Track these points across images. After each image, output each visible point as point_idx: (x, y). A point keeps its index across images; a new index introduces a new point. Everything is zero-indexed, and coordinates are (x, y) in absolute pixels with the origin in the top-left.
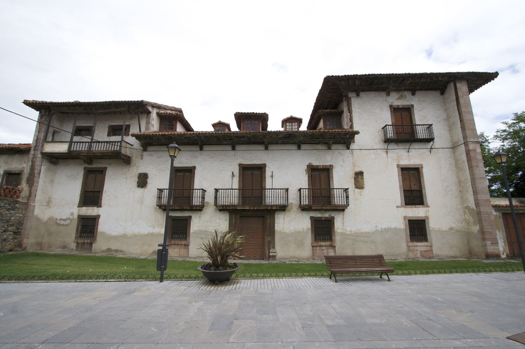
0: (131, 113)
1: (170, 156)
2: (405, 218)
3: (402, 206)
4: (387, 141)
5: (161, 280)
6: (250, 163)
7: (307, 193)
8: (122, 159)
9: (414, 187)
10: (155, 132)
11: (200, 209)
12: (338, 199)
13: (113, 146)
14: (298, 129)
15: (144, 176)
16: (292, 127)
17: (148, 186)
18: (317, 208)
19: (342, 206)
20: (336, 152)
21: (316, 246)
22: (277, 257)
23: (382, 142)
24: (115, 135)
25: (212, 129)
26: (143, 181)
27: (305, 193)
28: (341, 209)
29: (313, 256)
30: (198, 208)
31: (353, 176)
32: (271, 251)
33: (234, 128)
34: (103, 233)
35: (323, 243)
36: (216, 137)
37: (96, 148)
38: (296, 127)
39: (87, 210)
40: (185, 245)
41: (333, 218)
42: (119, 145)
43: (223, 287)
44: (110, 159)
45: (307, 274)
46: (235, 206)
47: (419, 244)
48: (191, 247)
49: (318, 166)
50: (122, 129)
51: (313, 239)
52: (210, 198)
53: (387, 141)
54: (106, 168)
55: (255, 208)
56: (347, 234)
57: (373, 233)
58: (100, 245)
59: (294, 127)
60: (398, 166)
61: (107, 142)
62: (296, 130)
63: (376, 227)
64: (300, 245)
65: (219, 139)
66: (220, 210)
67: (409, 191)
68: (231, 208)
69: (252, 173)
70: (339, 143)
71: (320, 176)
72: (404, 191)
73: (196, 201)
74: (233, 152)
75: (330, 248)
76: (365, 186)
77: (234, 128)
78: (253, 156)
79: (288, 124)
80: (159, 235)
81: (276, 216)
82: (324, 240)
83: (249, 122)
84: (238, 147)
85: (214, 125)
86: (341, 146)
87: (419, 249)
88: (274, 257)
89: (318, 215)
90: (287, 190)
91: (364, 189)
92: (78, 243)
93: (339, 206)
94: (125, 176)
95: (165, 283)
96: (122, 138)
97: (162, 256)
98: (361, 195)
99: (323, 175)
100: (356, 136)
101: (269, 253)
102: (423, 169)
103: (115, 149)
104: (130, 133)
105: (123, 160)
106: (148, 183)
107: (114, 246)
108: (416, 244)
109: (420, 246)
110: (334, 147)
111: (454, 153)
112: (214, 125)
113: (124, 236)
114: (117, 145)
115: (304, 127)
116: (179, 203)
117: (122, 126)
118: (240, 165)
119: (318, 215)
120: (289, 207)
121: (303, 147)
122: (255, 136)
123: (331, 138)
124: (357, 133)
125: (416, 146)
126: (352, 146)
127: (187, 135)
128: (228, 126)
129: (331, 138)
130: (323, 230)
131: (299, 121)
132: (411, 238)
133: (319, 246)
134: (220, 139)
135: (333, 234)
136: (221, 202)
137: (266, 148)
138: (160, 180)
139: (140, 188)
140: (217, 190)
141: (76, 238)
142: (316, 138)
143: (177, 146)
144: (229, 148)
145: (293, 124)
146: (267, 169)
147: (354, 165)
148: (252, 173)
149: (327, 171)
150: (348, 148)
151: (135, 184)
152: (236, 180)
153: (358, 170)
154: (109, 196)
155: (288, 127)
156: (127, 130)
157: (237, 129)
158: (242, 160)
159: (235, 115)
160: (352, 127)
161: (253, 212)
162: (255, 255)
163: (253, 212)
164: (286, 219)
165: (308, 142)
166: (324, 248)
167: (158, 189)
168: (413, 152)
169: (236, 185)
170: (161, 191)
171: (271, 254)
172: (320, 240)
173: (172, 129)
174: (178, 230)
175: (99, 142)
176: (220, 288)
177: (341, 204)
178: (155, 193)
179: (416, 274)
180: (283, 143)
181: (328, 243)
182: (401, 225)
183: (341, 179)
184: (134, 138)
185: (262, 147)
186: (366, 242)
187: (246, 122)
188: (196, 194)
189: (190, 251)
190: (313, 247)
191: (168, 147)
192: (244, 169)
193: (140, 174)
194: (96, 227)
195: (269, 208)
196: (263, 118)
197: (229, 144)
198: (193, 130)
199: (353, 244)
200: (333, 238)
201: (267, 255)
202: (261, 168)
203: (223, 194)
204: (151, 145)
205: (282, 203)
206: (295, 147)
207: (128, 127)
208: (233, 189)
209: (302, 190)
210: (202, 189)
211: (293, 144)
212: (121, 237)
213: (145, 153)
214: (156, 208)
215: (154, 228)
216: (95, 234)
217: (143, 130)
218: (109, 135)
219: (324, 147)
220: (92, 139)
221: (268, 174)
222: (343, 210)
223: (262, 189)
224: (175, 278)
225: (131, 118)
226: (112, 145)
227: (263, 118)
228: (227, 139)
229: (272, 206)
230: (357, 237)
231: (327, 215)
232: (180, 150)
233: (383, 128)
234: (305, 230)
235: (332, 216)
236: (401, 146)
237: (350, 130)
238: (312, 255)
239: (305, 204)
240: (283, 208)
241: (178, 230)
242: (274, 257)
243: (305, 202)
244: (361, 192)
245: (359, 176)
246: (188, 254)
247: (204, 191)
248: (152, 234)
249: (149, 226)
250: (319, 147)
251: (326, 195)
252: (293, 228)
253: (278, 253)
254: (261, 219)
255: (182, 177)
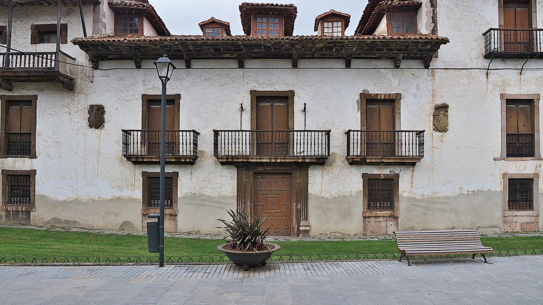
0: (66, 4)
1: (160, 77)
2: (504, 175)
3: (502, 159)
4: (490, 55)
5: (162, 265)
6: (268, 89)
7: (359, 137)
8: (61, 82)
9: (523, 130)
10: (109, 36)
11: (191, 161)
12: (407, 147)
13: (45, 60)
14: (343, 33)
15: (98, 110)
16: (334, 31)
17: (106, 125)
18: (373, 161)
19: (413, 158)
20: (408, 73)
21: (369, 217)
22: (312, 233)
23: (482, 57)
24: (41, 41)
25: (199, 32)
26: (97, 117)
27: (356, 137)
28: (410, 163)
29: (364, 230)
30: (188, 160)
31: (432, 111)
32: (302, 223)
33: (237, 30)
34: (44, 198)
35: (379, 213)
36: (213, 45)
37: (16, 63)
38: (340, 29)
39: (15, 162)
40: (171, 215)
41: (398, 176)
42: (53, 58)
43: (257, 274)
44: (41, 81)
45: (355, 256)
46: (246, 157)
47: (521, 213)
48: (179, 217)
49: (377, 94)
50: (55, 32)
51: (366, 207)
52: (206, 145)
53: (490, 55)
54: (36, 97)
55: (279, 161)
56: (417, 200)
57: (455, 198)
58: (41, 215)
59: (335, 30)
60: (502, 96)
61: (34, 54)
62: (340, 35)
63: (461, 188)
64: (346, 215)
65: (211, 49)
66: (223, 164)
67: (515, 135)
68: (240, 160)
69: (272, 105)
70: (412, 58)
71: (378, 108)
72: (508, 135)
73: (185, 150)
74: (240, 71)
75: (391, 219)
76: (449, 128)
77: (237, 30)
78: (274, 78)
79: (326, 24)
80: (219, 201)
81: (310, 172)
82: (382, 208)
83: (265, 20)
84: (249, 63)
85: (203, 26)
86: (415, 64)
87: (521, 220)
88: (307, 232)
89: (375, 171)
90: (328, 133)
91: (448, 132)
92: (8, 212)
93: (408, 158)
94: (67, 110)
95: (168, 268)
96: (58, 47)
97: (156, 232)
98: (442, 141)
99: (385, 110)
100: (442, 46)
101: (299, 226)
102: (540, 101)
103: (49, 66)
104: (70, 38)
105: (63, 83)
106: (106, 120)
107: (66, 215)
108: (516, 213)
109: (522, 217)
110: (404, 64)
111: (176, 69)
112: (203, 26)
113: (76, 202)
114: (51, 59)
115: (350, 32)
116: (159, 152)
117: (55, 26)
118: (252, 92)
119: (375, 171)
120: (331, 158)
121: (355, 63)
122: (277, 44)
123: (401, 50)
124: (445, 41)
125: (532, 64)
126: (434, 64)
127: (166, 43)
128: (226, 27)
129: (401, 50)
130: (381, 194)
131: (345, 20)
132: (509, 205)
133: (374, 217)
134: (220, 50)
135: (395, 198)
136: (222, 152)
137: (348, 65)
138: (126, 114)
139: (93, 129)
140: (216, 133)
141: (5, 203)
142: (377, 50)
143: (170, 61)
144: (234, 64)
145: (335, 24)
146: (296, 99)
147: (434, 95)
148: (272, 105)
149: (392, 102)
150: (427, 67)
151: (85, 123)
152: (247, 116)
153: (439, 102)
154: (45, 141)
155: (326, 30)
156: (63, 33)
157: (242, 33)
158: (256, 84)
159: (240, 8)
160: (434, 31)
161: (273, 165)
162: (277, 230)
163: (273, 165)
164: (326, 178)
165: (364, 56)
166: (381, 219)
167: (123, 131)
168: (528, 75)
169: (247, 126)
170: (127, 133)
171: (301, 228)
172: (376, 208)
173: (136, 31)
174: (159, 192)
175: (21, 54)
176: (252, 275)
177: (411, 154)
178: (120, 136)
179: (525, 253)
180: (323, 57)
181: (388, 213)
182: (499, 187)
183: (412, 116)
184: (77, 46)
185: (287, 64)
186: (444, 211)
187: (259, 20)
188: (181, 138)
189: (178, 224)
190: (365, 218)
191: (155, 64)
192: (259, 98)
193: (92, 107)
194: (32, 188)
195: (300, 161)
196: (288, 14)
197: (234, 58)
198: (169, 34)
199: (425, 214)
200: (396, 205)
201: (296, 230)
202: (287, 98)
203: (227, 138)
204: (105, 58)
205: (320, 153)
206: (341, 64)
207: (64, 27)
208: (242, 131)
209: (351, 133)
210: (194, 131)
211: (338, 58)
212: (72, 202)
213: (97, 73)
214: (121, 160)
215: (121, 190)
216: (32, 198)
217: (89, 33)
218: (34, 41)
219: (389, 64)
220: (9, 49)
221: (298, 107)
222: (414, 164)
223: (289, 130)
224: (179, 262)
225: (68, 13)
226: (43, 58)
227: (288, 14)
228: (230, 50)
229: (304, 157)
230: (430, 204)
231: (386, 171)
232: (174, 68)
233: (484, 34)
234: (353, 194)
235: (397, 172)
236: (510, 64)
237: (434, 37)
238: (362, 230)
239: (355, 154)
240: (321, 161)
241: (159, 192)
242: (307, 232)
243: (356, 151)
244: (442, 137)
245: (442, 109)
246: (176, 228)
247: (196, 133)
248: (119, 198)
249: (113, 188)
250: (379, 63)
251: (389, 142)
252: (335, 190)
253: (312, 226)
254: (286, 176)
255: (160, 109)
